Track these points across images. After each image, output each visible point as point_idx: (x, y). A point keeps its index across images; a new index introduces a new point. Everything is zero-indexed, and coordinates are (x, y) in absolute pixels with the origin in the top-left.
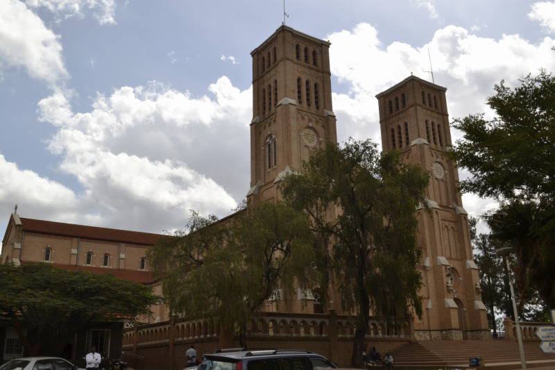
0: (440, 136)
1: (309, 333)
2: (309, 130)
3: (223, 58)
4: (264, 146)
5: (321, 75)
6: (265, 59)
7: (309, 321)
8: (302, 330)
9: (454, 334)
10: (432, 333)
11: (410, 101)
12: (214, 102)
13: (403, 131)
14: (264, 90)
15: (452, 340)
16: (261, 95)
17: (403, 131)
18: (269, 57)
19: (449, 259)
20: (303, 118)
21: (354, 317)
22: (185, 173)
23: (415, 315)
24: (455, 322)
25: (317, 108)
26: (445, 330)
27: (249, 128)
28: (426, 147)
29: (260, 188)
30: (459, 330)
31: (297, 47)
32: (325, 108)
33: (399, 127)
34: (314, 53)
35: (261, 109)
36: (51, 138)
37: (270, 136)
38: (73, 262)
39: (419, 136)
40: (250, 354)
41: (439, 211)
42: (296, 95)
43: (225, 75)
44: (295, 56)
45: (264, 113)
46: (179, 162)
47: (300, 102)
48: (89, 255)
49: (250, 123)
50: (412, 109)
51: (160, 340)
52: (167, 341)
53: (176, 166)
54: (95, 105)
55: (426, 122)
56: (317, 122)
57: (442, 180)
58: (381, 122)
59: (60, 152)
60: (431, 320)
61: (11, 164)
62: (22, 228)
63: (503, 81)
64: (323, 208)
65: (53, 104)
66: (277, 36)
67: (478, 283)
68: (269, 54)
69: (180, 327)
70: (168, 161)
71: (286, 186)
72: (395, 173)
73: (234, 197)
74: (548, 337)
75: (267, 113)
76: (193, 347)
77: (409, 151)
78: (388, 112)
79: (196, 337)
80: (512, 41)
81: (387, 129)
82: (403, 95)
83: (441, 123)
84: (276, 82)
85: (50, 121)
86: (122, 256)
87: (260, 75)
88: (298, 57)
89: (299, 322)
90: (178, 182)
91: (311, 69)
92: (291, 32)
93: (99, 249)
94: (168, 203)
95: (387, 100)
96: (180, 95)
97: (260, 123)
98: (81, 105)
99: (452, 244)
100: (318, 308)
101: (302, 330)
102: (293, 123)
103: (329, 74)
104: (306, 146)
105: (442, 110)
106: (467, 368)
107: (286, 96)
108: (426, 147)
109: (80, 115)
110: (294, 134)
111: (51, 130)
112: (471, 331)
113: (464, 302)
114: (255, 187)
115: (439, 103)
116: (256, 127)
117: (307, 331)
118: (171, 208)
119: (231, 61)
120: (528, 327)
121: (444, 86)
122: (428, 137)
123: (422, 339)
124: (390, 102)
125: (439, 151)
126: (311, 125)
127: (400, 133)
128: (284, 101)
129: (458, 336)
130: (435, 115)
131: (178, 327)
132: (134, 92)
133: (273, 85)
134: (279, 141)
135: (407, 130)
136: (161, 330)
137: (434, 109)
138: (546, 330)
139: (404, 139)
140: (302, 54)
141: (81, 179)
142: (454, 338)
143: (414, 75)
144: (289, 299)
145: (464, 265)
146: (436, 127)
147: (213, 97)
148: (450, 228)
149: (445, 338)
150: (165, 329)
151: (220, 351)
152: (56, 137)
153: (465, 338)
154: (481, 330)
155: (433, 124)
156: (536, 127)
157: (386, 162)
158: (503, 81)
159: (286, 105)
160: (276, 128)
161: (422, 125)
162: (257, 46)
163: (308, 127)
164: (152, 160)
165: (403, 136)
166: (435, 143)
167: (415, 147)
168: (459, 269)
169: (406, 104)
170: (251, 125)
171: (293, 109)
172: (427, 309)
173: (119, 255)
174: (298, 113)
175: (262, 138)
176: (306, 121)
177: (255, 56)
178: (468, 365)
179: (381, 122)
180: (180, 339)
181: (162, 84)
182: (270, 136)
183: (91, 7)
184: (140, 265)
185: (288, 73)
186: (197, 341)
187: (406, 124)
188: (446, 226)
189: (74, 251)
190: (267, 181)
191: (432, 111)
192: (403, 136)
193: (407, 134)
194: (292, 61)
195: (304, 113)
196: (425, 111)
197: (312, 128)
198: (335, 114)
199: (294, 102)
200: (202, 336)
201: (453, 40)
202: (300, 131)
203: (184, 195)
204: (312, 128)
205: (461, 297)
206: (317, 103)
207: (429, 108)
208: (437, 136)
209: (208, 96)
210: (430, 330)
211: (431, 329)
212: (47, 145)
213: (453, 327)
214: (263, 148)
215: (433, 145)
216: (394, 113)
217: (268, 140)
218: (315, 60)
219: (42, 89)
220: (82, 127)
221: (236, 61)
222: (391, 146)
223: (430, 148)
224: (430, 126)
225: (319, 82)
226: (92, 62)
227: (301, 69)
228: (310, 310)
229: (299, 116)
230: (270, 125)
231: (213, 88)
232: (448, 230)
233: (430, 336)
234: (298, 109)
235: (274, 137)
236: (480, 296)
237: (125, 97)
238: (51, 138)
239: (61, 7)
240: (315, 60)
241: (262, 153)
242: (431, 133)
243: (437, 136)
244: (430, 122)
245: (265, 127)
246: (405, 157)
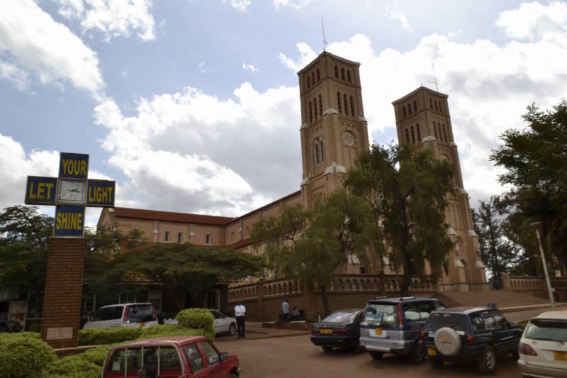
0: (445, 134)
1: (352, 288)
3: (244, 66)
5: (354, 89)
6: (310, 78)
7: (358, 279)
8: (354, 287)
11: (420, 107)
12: (238, 105)
13: (415, 130)
16: (308, 108)
17: (415, 130)
18: (313, 76)
19: (456, 229)
20: (343, 124)
21: (401, 276)
22: (209, 164)
23: (444, 274)
24: (463, 278)
25: (353, 115)
27: (299, 133)
28: (435, 143)
29: (311, 179)
30: (466, 283)
31: (336, 68)
32: (359, 115)
33: (412, 128)
34: (349, 72)
35: (309, 117)
37: (318, 139)
38: (155, 240)
39: (429, 134)
40: (402, 300)
42: (337, 106)
43: (250, 82)
44: (334, 75)
45: (311, 121)
46: (205, 156)
47: (340, 112)
48: (167, 234)
49: (300, 128)
50: (422, 114)
51: (249, 297)
52: (256, 297)
53: (201, 159)
54: (140, 109)
55: (434, 122)
56: (354, 127)
57: (353, 147)
62: (115, 215)
63: (534, 103)
65: (106, 109)
67: (478, 248)
68: (313, 74)
70: (195, 156)
71: (346, 179)
72: (428, 167)
73: (249, 183)
75: (314, 120)
76: (286, 301)
77: (421, 146)
78: (402, 116)
79: (282, 294)
80: (484, 45)
83: (444, 122)
85: (104, 123)
86: (192, 234)
88: (337, 75)
90: (202, 171)
91: (348, 85)
93: (174, 229)
94: (196, 190)
95: (401, 106)
96: (211, 98)
97: (308, 128)
98: (129, 110)
99: (457, 218)
100: (363, 270)
101: (354, 287)
102: (336, 127)
103: (449, 117)
104: (346, 146)
105: (355, 83)
107: (330, 107)
108: (435, 143)
109: (128, 120)
110: (337, 137)
111: (104, 131)
112: (474, 285)
113: (467, 262)
114: (306, 179)
115: (443, 108)
116: (305, 133)
117: (357, 287)
118: (198, 193)
119: (250, 69)
121: (357, 61)
122: (436, 135)
124: (404, 107)
125: (444, 145)
126: (349, 129)
127: (413, 132)
129: (465, 288)
130: (440, 117)
131: (265, 287)
132: (173, 98)
134: (327, 143)
135: (418, 129)
136: (249, 290)
137: (439, 112)
139: (416, 137)
140: (340, 74)
141: (127, 172)
143: (424, 85)
145: (467, 233)
147: (237, 100)
150: (253, 289)
151: (375, 299)
152: (109, 137)
153: (470, 290)
154: (460, 284)
155: (439, 124)
157: (403, 153)
158: (534, 103)
159: (330, 115)
160: (322, 133)
161: (431, 126)
163: (347, 131)
164: (183, 154)
165: (416, 135)
166: (441, 139)
168: (463, 237)
173: (189, 234)
174: (340, 120)
175: (311, 139)
176: (345, 127)
177: (302, 75)
179: (301, 96)
180: (267, 296)
181: (195, 90)
182: (318, 139)
183: (134, 27)
184: (205, 241)
185: (329, 91)
186: (289, 296)
187: (418, 125)
189: (156, 231)
190: (317, 174)
191: (438, 114)
192: (416, 135)
193: (419, 133)
194: (332, 79)
195: (344, 120)
196: (432, 114)
197: (350, 131)
198: (366, 120)
199: (336, 111)
200: (288, 293)
201: (436, 47)
202: (341, 134)
203: (209, 182)
204: (350, 131)
205: (465, 259)
206: (352, 111)
208: (442, 133)
209: (233, 99)
212: (102, 143)
215: (440, 141)
216: (407, 116)
217: (316, 142)
218: (349, 78)
220: (129, 128)
221: (255, 68)
222: (405, 139)
223: (439, 144)
224: (437, 126)
225: (353, 95)
226: (124, 74)
227: (340, 85)
228: (357, 271)
230: (317, 130)
231: (237, 92)
233: (444, 289)
235: (320, 139)
236: (480, 258)
237: (163, 102)
239: (111, 27)
240: (349, 78)
241: (311, 152)
242: (438, 131)
243: (442, 133)
244: (437, 123)
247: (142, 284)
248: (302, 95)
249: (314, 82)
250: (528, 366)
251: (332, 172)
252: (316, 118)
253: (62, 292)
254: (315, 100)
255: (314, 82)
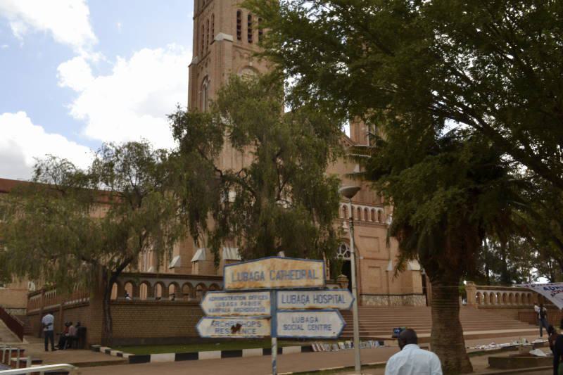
2: (249, 70)
4: (201, 90)
9: (414, 300)
10: (391, 297)
14: (203, 27)
15: (413, 306)
26: (407, 295)
35: (200, 48)
36: (72, 103)
37: (206, 77)
45: (202, 53)
47: (239, 39)
59: (82, 117)
61: (37, 127)
64: (216, 151)
74: (218, 310)
75: (205, 52)
84: (213, 16)
89: (194, 285)
97: (198, 64)
98: (100, 70)
107: (221, 31)
120: (520, 293)
123: (379, 305)
126: (251, 64)
128: (220, 36)
133: (211, 20)
138: (216, 298)
142: (415, 304)
144: (187, 256)
149: (405, 304)
156: (341, 29)
171: (228, 46)
172: (387, 271)
178: (390, 336)
199: (230, 37)
210: (389, 295)
211: (391, 293)
213: (415, 292)
214: (199, 92)
217: (205, 83)
219: (66, 53)
226: (119, 25)
229: (237, 54)
233: (389, 301)
234: (234, 46)
238: (72, 103)
245: (202, 68)
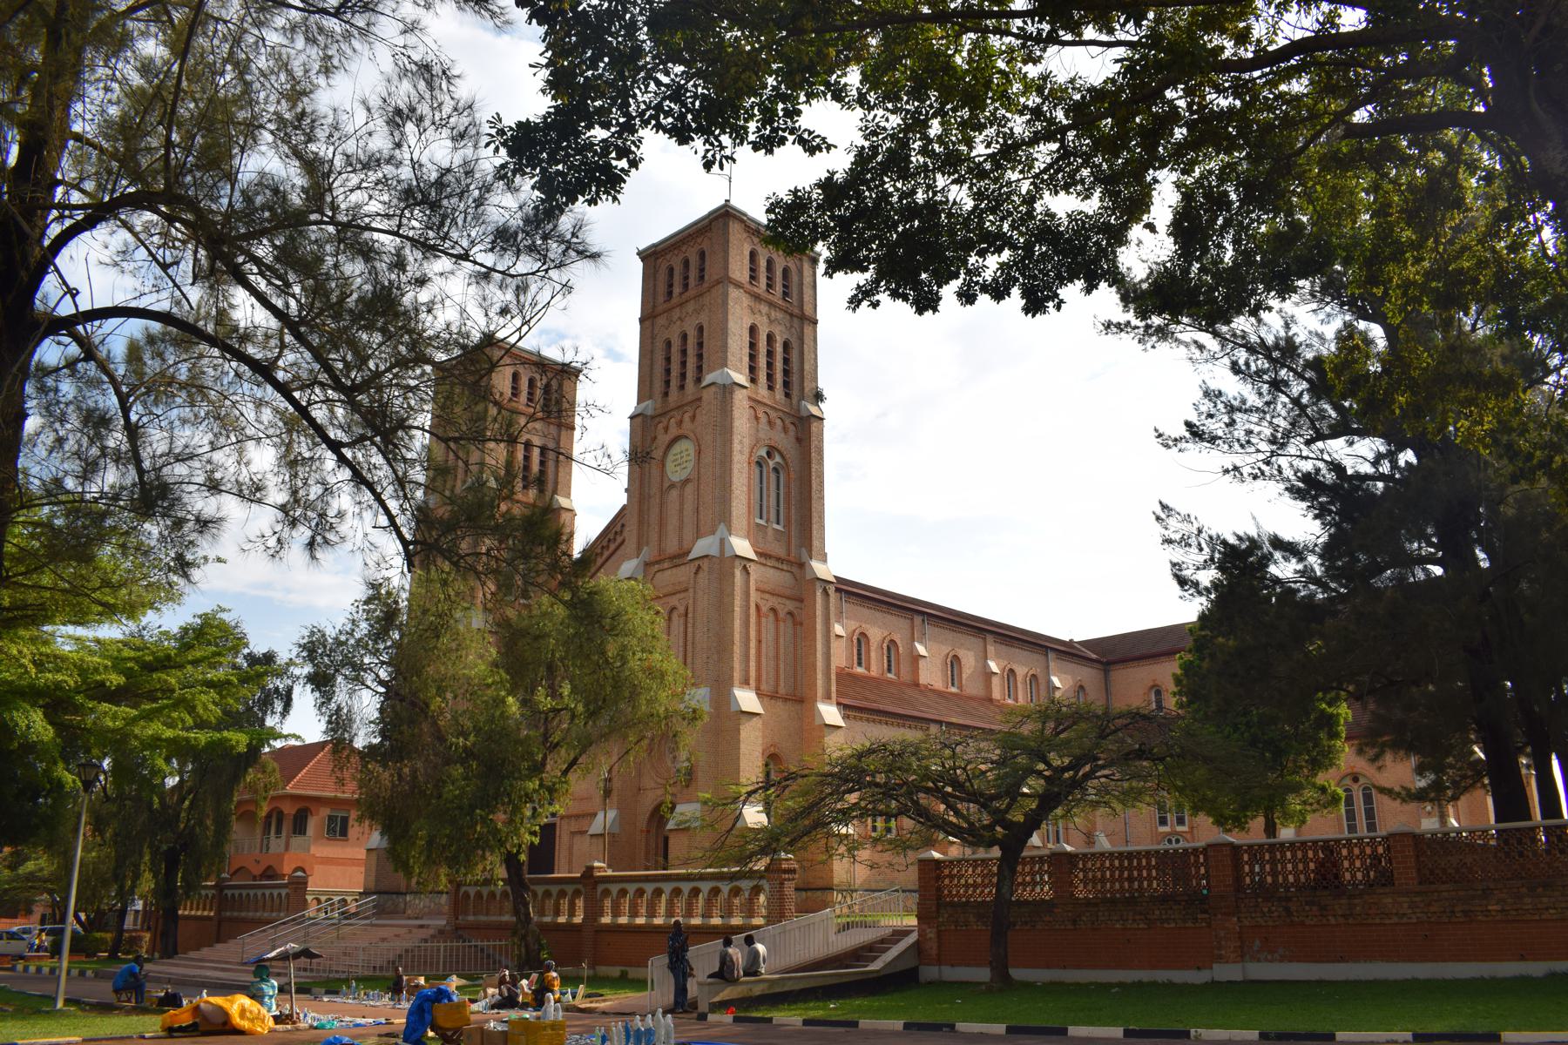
17: (692, 341)
35: (658, 385)
41: (752, 568)
45: (666, 394)
58: (642, 320)
60: (819, 893)
66: (711, 222)
68: (686, 263)
69: (472, 895)
81: (653, 338)
82: (702, 255)
87: (660, 309)
92: (742, 221)
97: (653, 417)
106: (894, 1034)
146: (779, 349)
148: (782, 614)
162: (655, 241)
165: (691, 362)
167: (713, 389)
169: (706, 278)
170: (631, 418)
188: (773, 610)
191: (771, 304)
192: (691, 362)
206: (786, 384)
207: (765, 295)
215: (762, 392)
232: (777, 619)
242: (762, 361)
246: (687, 417)
247: (160, 928)
248: (648, 318)
249: (686, 286)
250: (821, 1004)
251: (714, 551)
252: (682, 387)
253: (371, 1020)
254: (684, 337)
255: (686, 286)
